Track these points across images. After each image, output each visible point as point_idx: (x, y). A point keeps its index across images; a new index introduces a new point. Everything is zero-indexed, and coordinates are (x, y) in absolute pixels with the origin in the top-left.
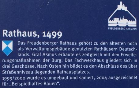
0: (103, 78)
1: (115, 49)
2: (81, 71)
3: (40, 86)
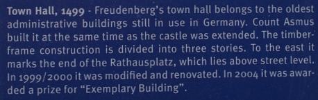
0: (250, 74)
1: (219, 23)
2: (166, 60)
3: (128, 95)
